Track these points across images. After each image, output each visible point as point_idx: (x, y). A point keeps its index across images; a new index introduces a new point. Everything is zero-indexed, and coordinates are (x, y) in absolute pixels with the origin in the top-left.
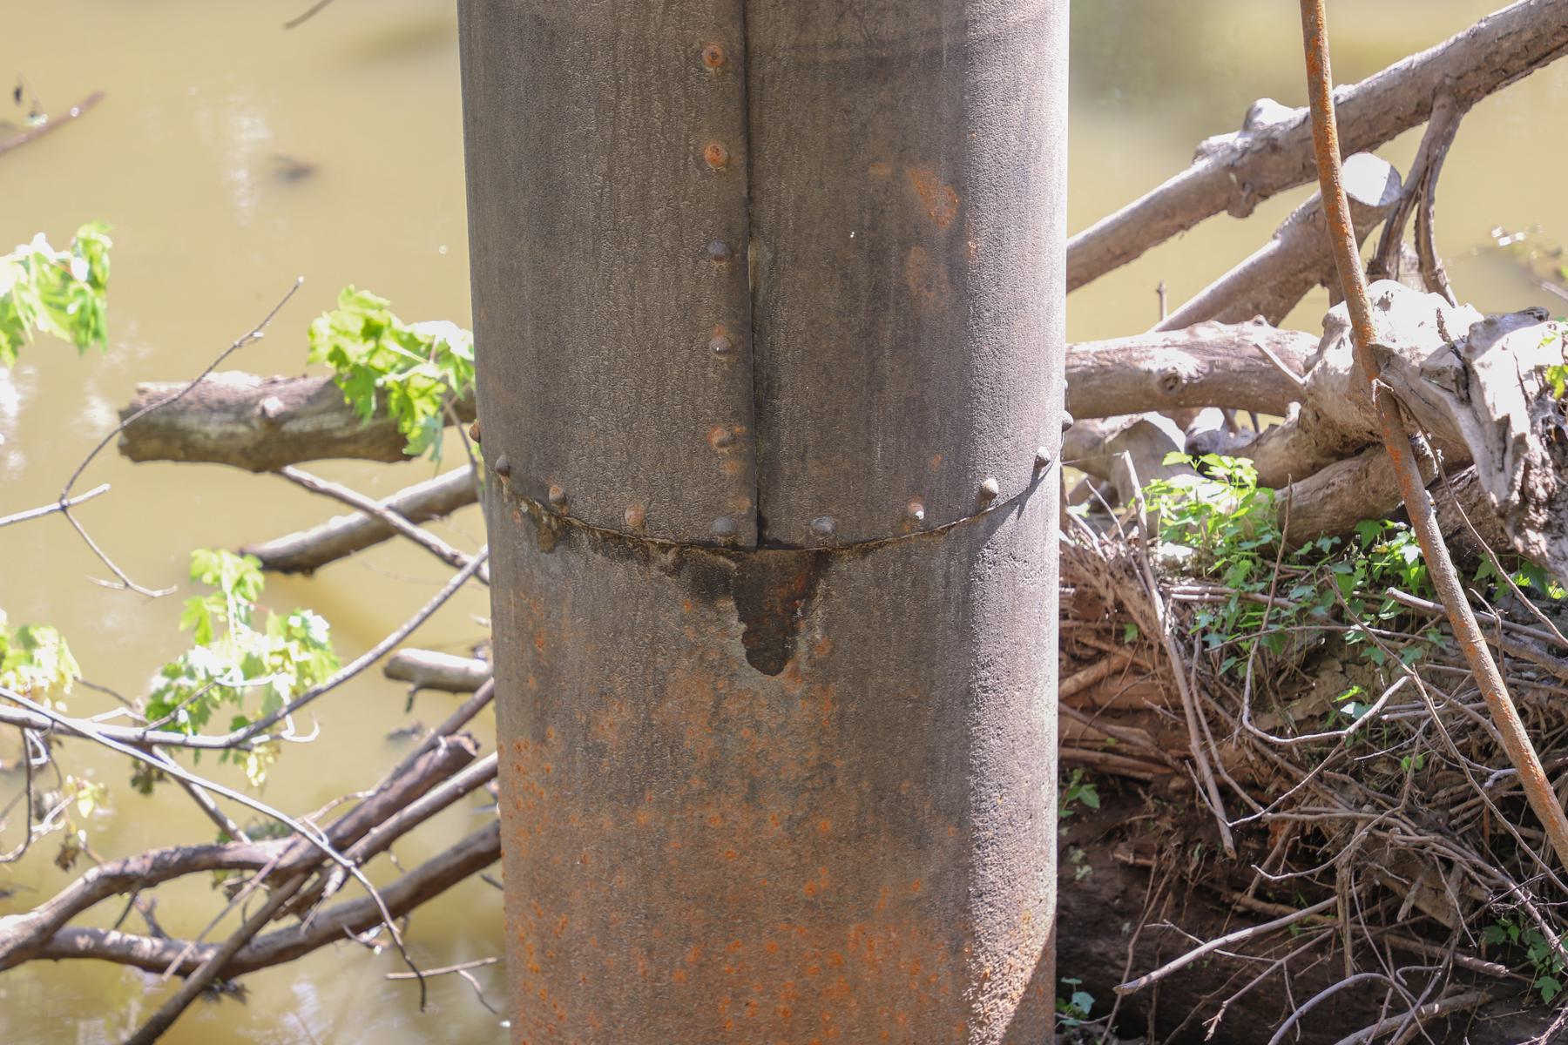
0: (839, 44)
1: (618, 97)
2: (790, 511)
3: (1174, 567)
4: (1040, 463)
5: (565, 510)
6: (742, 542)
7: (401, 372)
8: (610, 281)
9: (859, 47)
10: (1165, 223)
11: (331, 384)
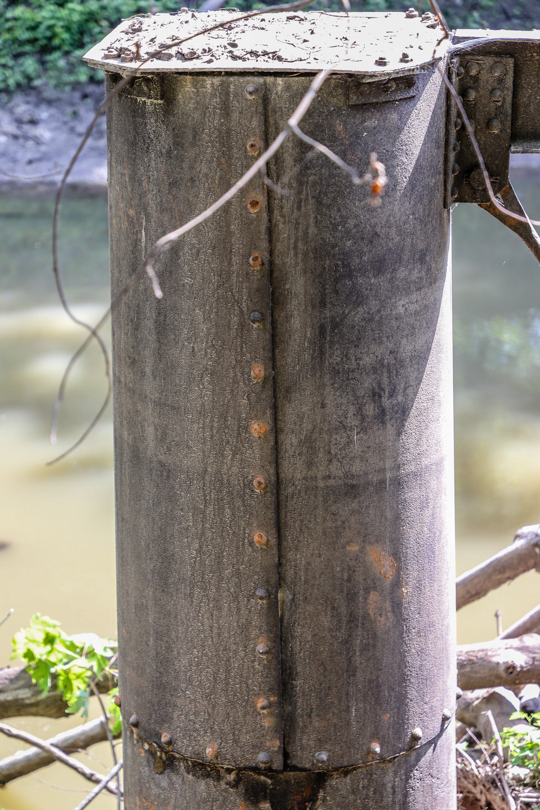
0: (329, 477)
1: (205, 506)
2: (302, 748)
3: (519, 781)
4: (445, 719)
5: (170, 748)
6: (275, 767)
7: (66, 664)
8: (199, 612)
9: (340, 478)
10: (500, 576)
11: (24, 671)
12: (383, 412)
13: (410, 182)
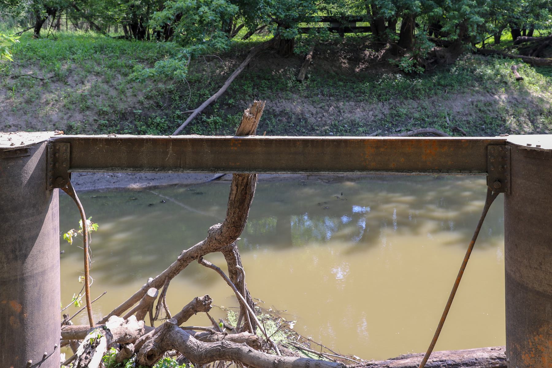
12: (16, 256)
13: (28, 182)
